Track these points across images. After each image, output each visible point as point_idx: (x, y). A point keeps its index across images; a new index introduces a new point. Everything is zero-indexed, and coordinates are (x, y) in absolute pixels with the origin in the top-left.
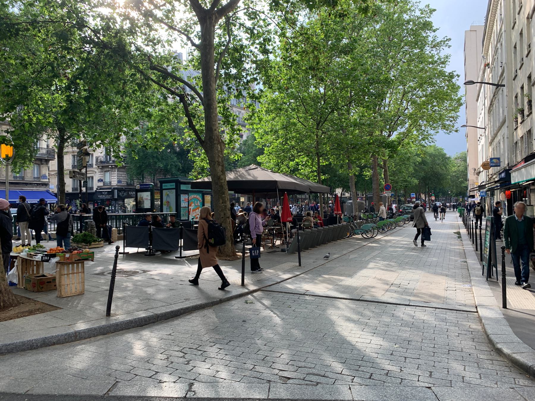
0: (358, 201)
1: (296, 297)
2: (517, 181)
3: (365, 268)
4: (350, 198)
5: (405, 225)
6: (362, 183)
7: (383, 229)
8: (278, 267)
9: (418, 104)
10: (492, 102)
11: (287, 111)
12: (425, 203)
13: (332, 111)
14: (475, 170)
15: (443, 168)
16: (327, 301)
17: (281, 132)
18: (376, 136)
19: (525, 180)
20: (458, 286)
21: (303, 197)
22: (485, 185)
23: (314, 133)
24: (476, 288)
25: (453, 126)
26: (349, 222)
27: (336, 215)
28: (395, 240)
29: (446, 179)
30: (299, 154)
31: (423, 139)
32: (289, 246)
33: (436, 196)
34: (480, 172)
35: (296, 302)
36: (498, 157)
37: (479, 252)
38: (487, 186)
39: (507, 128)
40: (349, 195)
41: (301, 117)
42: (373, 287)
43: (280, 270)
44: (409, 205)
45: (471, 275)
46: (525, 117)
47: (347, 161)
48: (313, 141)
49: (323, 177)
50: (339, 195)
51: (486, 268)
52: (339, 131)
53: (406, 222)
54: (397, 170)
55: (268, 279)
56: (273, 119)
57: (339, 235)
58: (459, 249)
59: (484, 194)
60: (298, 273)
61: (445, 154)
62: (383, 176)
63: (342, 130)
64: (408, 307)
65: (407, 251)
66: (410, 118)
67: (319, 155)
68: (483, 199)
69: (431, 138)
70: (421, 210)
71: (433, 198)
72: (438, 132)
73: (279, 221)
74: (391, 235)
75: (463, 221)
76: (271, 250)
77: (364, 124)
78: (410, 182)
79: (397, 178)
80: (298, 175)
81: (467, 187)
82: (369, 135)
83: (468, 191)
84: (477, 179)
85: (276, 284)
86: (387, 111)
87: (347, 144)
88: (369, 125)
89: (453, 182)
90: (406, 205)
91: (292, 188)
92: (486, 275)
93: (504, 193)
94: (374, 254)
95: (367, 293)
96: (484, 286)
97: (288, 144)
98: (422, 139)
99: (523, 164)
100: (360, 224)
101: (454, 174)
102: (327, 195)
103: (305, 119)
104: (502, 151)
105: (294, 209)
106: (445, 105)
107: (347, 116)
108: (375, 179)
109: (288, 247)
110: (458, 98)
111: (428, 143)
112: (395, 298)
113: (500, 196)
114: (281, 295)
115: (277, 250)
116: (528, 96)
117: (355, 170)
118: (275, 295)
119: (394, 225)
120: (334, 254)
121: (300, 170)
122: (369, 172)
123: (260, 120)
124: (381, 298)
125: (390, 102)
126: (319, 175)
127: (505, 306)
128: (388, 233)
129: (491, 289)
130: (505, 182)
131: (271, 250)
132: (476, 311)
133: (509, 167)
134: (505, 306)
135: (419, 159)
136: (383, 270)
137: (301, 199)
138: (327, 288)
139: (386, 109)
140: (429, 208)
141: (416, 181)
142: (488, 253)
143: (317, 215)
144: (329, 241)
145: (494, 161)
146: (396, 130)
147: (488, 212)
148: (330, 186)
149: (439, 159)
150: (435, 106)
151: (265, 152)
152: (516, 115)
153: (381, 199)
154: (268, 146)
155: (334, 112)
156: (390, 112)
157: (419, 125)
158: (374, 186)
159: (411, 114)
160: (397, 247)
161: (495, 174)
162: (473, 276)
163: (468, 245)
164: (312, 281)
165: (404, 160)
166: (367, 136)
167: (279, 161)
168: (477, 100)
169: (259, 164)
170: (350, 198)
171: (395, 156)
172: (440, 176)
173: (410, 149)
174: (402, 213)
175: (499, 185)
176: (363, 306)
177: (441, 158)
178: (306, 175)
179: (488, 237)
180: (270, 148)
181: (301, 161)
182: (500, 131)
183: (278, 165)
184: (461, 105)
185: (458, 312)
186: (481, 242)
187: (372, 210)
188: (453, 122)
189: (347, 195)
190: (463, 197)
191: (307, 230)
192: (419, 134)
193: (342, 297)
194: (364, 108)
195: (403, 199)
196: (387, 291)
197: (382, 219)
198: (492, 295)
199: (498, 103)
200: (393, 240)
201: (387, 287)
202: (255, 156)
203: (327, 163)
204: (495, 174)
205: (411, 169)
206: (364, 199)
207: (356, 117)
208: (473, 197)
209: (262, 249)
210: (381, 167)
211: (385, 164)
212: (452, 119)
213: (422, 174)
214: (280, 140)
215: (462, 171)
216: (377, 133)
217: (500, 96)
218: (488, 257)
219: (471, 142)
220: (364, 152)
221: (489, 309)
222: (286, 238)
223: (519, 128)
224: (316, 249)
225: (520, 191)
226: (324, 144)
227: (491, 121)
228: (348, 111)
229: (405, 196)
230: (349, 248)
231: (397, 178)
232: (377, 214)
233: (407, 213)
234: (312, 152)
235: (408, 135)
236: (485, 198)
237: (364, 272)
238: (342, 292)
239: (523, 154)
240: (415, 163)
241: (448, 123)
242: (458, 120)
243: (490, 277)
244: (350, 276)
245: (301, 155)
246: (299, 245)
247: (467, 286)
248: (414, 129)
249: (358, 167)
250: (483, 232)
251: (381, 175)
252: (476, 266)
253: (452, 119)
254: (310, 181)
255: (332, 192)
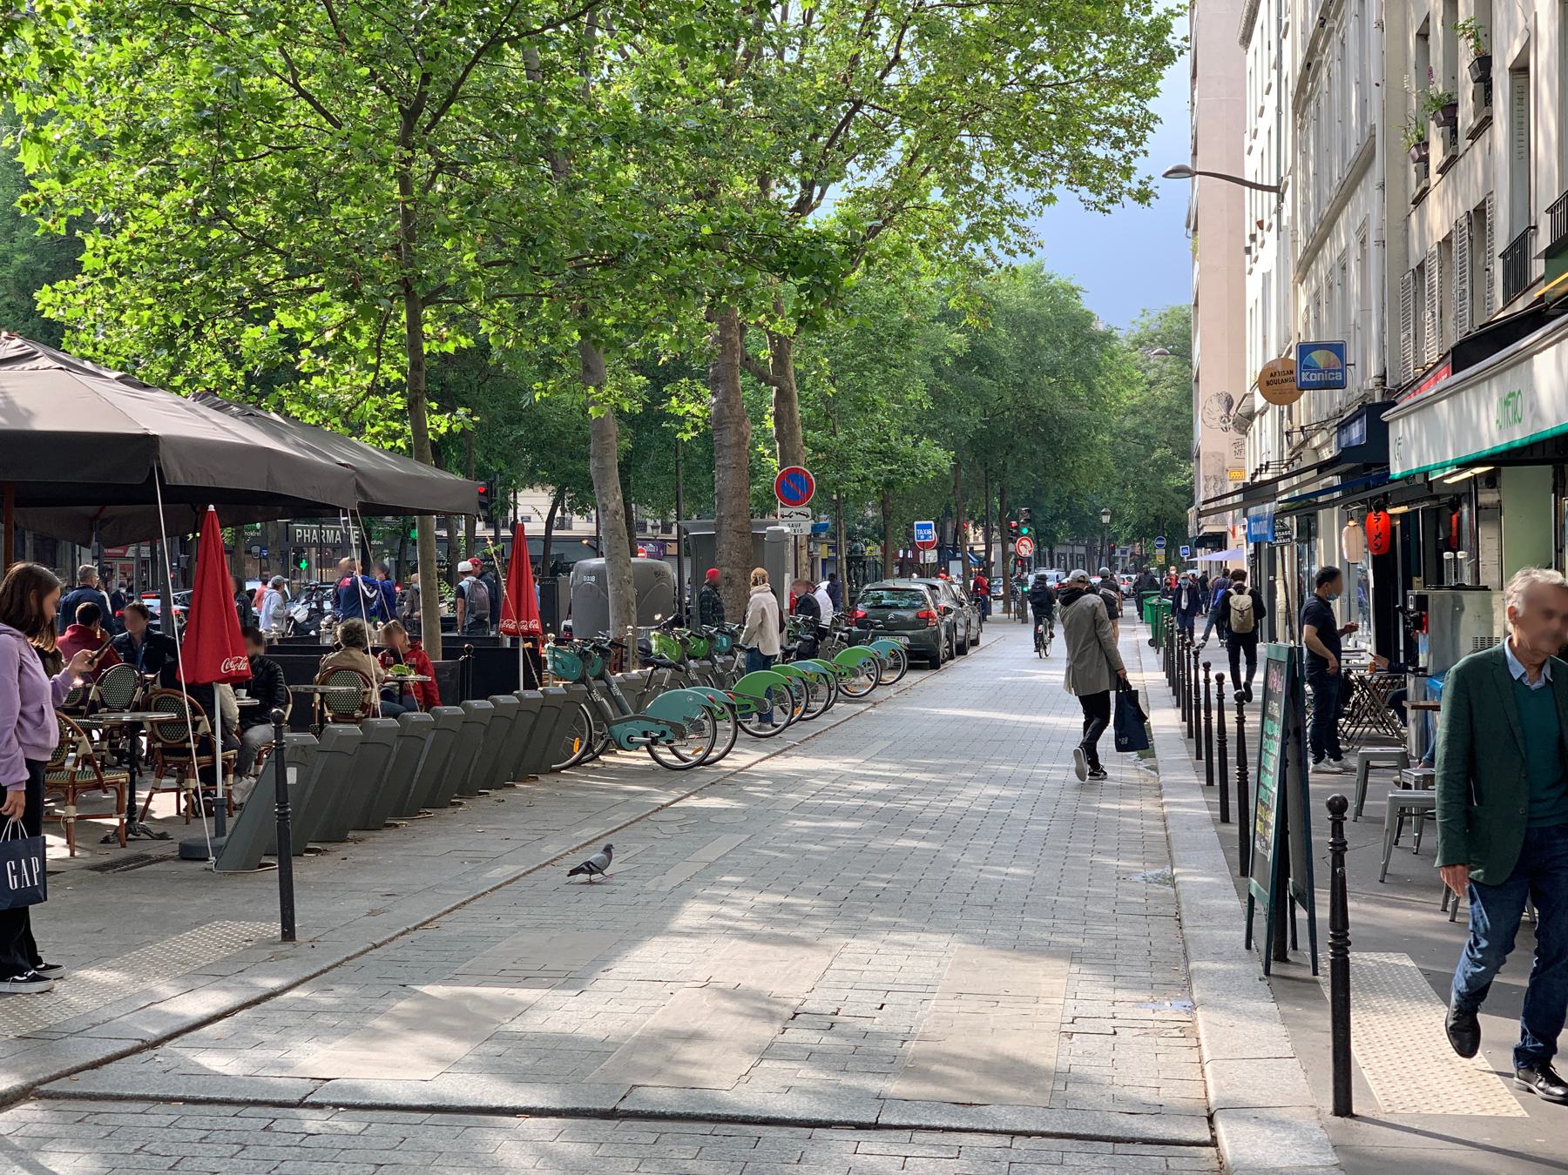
0: (641, 558)
1: (254, 1119)
2: (1414, 465)
3: (660, 930)
4: (594, 547)
5: (879, 693)
6: (657, 463)
7: (766, 718)
8: (155, 950)
9: (955, 41)
10: (1312, 52)
11: (222, 26)
12: (986, 572)
13: (492, 48)
14: (1229, 403)
15: (1079, 390)
16: (435, 1132)
17: (185, 147)
18: (734, 203)
19: (1450, 457)
20: (1125, 1011)
21: (331, 534)
22: (1275, 481)
23: (383, 164)
24: (1217, 1017)
25: (1127, 172)
26: (582, 680)
27: (515, 642)
28: (827, 773)
29: (1089, 448)
30: (301, 282)
31: (977, 233)
32: (230, 823)
33: (1044, 539)
34: (1251, 416)
35: (250, 1153)
36: (1338, 338)
37: (1234, 829)
38: (1282, 486)
39: (1377, 194)
40: (593, 527)
41: (312, 69)
42: (693, 1037)
43: (162, 969)
44: (901, 584)
45: (1192, 952)
46: (1463, 143)
47: (576, 335)
48: (379, 208)
49: (440, 424)
50: (535, 527)
51: (1261, 908)
52: (530, 162)
53: (888, 677)
54: (843, 393)
55: (89, 1027)
56: (141, 66)
57: (528, 755)
58: (1141, 814)
59: (1262, 529)
60: (273, 983)
61: (1089, 317)
62: (770, 424)
63: (549, 156)
64: (873, 1134)
65: (880, 832)
66: (911, 115)
67: (415, 293)
68: (1263, 555)
69: (1016, 229)
70: (1094, 609)
71: (1026, 548)
72: (1049, 199)
73: (170, 680)
74: (804, 746)
75: (1169, 667)
76: (116, 853)
77: (665, 133)
78: (908, 463)
79: (842, 436)
80: (294, 409)
81: (1188, 493)
82: (698, 196)
83: (1191, 513)
84: (1239, 448)
85: (137, 1050)
86: (796, 68)
87: (574, 241)
88: (697, 140)
89: (1122, 463)
90: (890, 583)
91: (256, 484)
92: (1263, 945)
93: (1362, 521)
94: (709, 853)
95: (657, 1072)
96: (1254, 1005)
97: (230, 217)
98: (971, 229)
99: (1446, 379)
100: (641, 692)
101: (1128, 424)
102: (471, 528)
103: (337, 77)
104: (1354, 308)
105: (273, 607)
106: (1090, 53)
107: (575, 82)
108: (730, 438)
109: (220, 830)
110: (1153, 22)
111: (1000, 253)
112: (804, 1091)
113: (1342, 543)
114: (161, 1115)
115: (155, 849)
116: (1475, 36)
117: (615, 392)
118: (122, 1119)
119: (823, 691)
120: (495, 860)
121: (308, 377)
122: (698, 398)
123: (56, 67)
124: (730, 1097)
125: (808, 22)
126: (413, 411)
127: (1343, 1106)
128: (790, 736)
129: (1285, 1019)
130: (1362, 469)
131: (116, 853)
132: (1208, 1138)
133: (1385, 393)
134: (1343, 1106)
135: (957, 341)
136: (752, 937)
137: (321, 546)
138: (440, 1060)
139: (790, 56)
140: (1006, 599)
141: (939, 457)
142: (1271, 833)
143: (402, 641)
144: (469, 790)
145: (1318, 357)
146: (839, 176)
147: (1289, 620)
148: (482, 473)
149: (1055, 342)
150: (1038, 57)
151: (88, 260)
152: (1423, 126)
153: (757, 549)
154: (105, 228)
155: (499, 54)
156: (809, 75)
157: (958, 158)
158: (723, 479)
159: (918, 95)
160: (834, 812)
161: (1321, 426)
162: (1201, 956)
163: (1189, 787)
164: (354, 1024)
165: (880, 340)
166: (685, 201)
167: (177, 319)
168: (1246, 39)
169: (51, 334)
170: (594, 547)
171: (829, 315)
172: (1062, 429)
173: (910, 283)
174: (866, 629)
175: (1336, 481)
176: (633, 1144)
177: (1063, 331)
178: (345, 418)
179: (1275, 748)
180: (122, 239)
181: (311, 326)
182: (1349, 208)
183: (169, 342)
184: (1167, 57)
185: (1120, 1147)
186: (1243, 775)
187: (711, 609)
188: (1128, 147)
189: (581, 526)
190: (1171, 547)
191: (341, 728)
192: (956, 205)
193: (520, 1102)
194: (665, 40)
195: (873, 551)
196: (767, 1052)
197: (759, 661)
198: (1286, 1049)
199: (1342, 60)
200: (816, 774)
201: (766, 1032)
202: (28, 283)
203: (464, 342)
204: (1321, 426)
205: (917, 392)
206: (673, 549)
207: (625, 87)
208: (1218, 541)
209: (56, 848)
210: (762, 377)
211: (780, 358)
212: (1122, 133)
213: (973, 420)
214: (181, 193)
215: (1168, 409)
216: (742, 186)
217: (1352, 26)
218: (1270, 854)
219: (1199, 258)
220: (664, 286)
221: (1272, 1122)
222: (208, 776)
223: (1432, 197)
224: (390, 834)
225: (1435, 516)
226: (445, 235)
227: (1305, 154)
228: (581, 51)
229: (883, 536)
230: (579, 825)
231: (842, 436)
232: (733, 636)
233: (891, 629)
234: (372, 277)
235: (899, 208)
236: (1272, 551)
237: (650, 956)
238: (521, 1077)
239: (1450, 326)
240: (934, 360)
241: (1100, 151)
242: (1152, 140)
243: (1282, 957)
244: (574, 980)
245: (312, 291)
246: (283, 816)
247: (1170, 1010)
248: (933, 176)
249: (640, 368)
250: (1253, 720)
251: (759, 420)
252: (1218, 902)
253: (1122, 133)
254: (365, 442)
255: (494, 506)
